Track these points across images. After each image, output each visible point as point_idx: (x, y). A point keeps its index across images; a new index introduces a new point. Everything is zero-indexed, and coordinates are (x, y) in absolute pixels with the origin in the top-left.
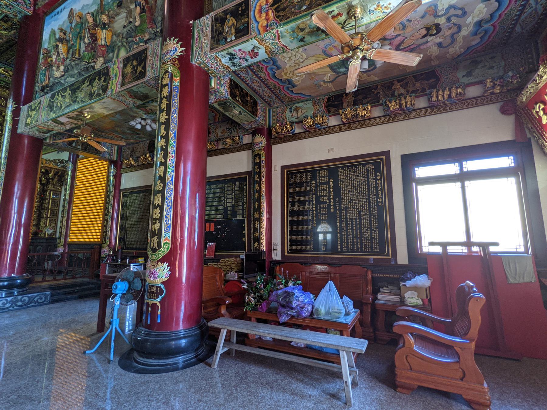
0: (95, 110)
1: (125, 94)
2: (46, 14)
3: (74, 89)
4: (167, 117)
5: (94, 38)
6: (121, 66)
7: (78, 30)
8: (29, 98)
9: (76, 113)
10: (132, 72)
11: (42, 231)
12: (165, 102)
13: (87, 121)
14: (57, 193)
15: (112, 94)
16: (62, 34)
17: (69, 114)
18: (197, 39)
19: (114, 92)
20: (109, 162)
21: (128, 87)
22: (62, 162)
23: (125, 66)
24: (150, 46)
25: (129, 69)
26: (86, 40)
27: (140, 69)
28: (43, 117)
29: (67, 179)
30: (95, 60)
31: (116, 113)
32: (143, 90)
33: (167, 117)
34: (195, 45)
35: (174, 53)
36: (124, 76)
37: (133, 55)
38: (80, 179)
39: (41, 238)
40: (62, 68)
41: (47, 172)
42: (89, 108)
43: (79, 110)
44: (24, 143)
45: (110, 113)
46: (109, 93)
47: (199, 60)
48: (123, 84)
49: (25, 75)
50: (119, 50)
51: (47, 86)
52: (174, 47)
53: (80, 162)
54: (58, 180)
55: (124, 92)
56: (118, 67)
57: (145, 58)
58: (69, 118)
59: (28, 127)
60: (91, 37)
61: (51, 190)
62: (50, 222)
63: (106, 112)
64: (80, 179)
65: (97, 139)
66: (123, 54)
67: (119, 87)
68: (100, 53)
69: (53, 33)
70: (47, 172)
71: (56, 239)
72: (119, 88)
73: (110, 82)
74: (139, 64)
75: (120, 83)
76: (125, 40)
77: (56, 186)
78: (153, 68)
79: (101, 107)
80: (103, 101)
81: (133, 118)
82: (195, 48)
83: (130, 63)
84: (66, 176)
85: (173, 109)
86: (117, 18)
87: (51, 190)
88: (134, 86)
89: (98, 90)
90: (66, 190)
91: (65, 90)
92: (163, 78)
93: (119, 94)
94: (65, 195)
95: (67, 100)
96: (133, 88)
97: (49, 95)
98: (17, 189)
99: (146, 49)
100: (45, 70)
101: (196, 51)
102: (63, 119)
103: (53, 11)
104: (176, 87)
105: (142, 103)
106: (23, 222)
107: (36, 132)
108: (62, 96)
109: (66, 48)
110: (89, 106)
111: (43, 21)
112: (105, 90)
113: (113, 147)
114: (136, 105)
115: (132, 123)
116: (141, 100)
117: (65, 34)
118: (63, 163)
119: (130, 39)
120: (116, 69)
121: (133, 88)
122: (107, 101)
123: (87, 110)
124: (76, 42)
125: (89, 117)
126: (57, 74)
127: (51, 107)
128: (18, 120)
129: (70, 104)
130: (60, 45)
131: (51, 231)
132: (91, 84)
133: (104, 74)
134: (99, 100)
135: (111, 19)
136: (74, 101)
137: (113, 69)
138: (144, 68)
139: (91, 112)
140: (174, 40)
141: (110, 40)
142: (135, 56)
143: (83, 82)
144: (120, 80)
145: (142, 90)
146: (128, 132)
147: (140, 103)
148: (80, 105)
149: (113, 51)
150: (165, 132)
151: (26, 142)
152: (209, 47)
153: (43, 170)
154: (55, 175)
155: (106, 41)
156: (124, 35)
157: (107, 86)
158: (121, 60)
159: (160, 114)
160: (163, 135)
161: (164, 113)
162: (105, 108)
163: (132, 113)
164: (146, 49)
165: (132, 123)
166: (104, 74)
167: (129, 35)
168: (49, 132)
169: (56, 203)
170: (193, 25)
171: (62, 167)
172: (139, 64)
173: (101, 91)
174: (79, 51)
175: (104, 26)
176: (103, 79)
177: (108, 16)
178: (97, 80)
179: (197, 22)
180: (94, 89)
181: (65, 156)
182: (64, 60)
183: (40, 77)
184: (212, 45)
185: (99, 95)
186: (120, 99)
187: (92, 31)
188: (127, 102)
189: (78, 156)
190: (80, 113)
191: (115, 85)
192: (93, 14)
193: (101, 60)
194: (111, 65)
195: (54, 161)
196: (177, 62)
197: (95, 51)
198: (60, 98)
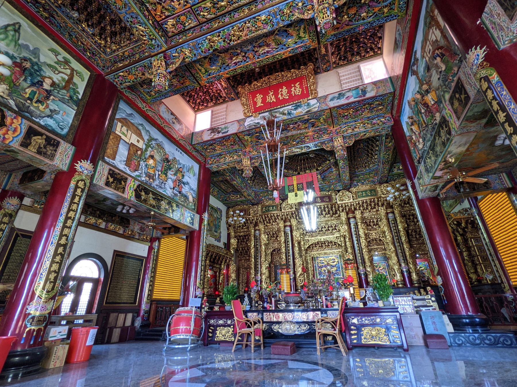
0: (454, 152)
1: (466, 124)
2: (399, 116)
3: (432, 148)
4: (505, 114)
5: (426, 105)
6: (450, 107)
7: (416, 109)
8: (415, 173)
9: (443, 164)
10: (459, 104)
11: (482, 277)
12: (494, 103)
13: (455, 165)
14: (478, 239)
15: (456, 132)
16: (411, 120)
17: (439, 167)
18: (492, 28)
19: (456, 129)
20: (506, 192)
21: (463, 117)
22: (466, 210)
23: (452, 104)
24: (461, 74)
25: (456, 104)
26: (423, 111)
27: (463, 97)
28: (427, 180)
29: (478, 224)
30: (434, 118)
31: (471, 145)
32: (478, 109)
33: (505, 114)
34: (494, 33)
35: (478, 60)
36: (456, 112)
37: (453, 92)
38: (489, 219)
39: (485, 285)
40: (421, 140)
41: (459, 224)
42: (449, 153)
43: (443, 160)
44: (427, 204)
45: (466, 147)
46: (453, 133)
47: (506, 41)
48: (458, 118)
49: (407, 160)
50: (444, 97)
51: (420, 158)
52: (477, 54)
53: (481, 204)
54: (472, 228)
55: (464, 123)
56: (449, 110)
57: (462, 85)
58: (441, 170)
59: (423, 192)
60: (424, 106)
61: (471, 238)
62: (485, 268)
63: (463, 149)
64: (489, 219)
65: (471, 174)
66: (447, 96)
67: (457, 122)
68: (434, 110)
69: (407, 123)
70: (459, 224)
71: (498, 284)
72: (458, 123)
73: (450, 124)
74: (460, 94)
75: (456, 120)
76: (444, 87)
77: (473, 234)
78: (471, 86)
79: (456, 147)
80: (453, 142)
81: (495, 138)
82: (495, 36)
83: (455, 99)
84: (476, 222)
85: (506, 103)
86: (432, 79)
87: (471, 238)
88: (467, 112)
89: (446, 135)
90: (482, 233)
91: (428, 152)
92: (481, 86)
93: (461, 127)
94: (484, 239)
95: (433, 158)
96: (467, 115)
97: (423, 163)
98: (438, 239)
99: (459, 79)
100: (414, 149)
101: (498, 37)
102: (439, 174)
103: (401, 111)
104: (497, 82)
105: (487, 119)
106: (457, 270)
107: (430, 193)
108: (429, 158)
109: (417, 126)
110: (447, 153)
111: (400, 120)
112: (449, 133)
113: (500, 176)
114: (483, 125)
115: (499, 142)
116: (484, 118)
117: (412, 118)
118: (468, 211)
119: (447, 83)
120: (448, 112)
121: (467, 115)
122: (456, 139)
123: (449, 156)
124: (419, 117)
125: (453, 161)
126: (420, 146)
127: (427, 171)
128: (416, 191)
129: (436, 160)
130: (413, 127)
131: (491, 277)
132: (440, 136)
133: (443, 123)
134: (450, 143)
135: (429, 83)
136: (437, 156)
137: (447, 113)
138: (466, 93)
139: (452, 156)
140: (471, 51)
141: (435, 97)
142: (454, 92)
143: (435, 138)
144: (455, 117)
145: (476, 110)
146: (504, 153)
147: (484, 121)
148: (442, 156)
149: (441, 102)
150: (512, 128)
151: (428, 203)
152: (507, 20)
153: (455, 223)
154: (467, 223)
155: (433, 100)
156: (442, 84)
157: (450, 129)
158: (447, 102)
159: (497, 116)
160: (512, 132)
161: (500, 112)
162: (460, 146)
163: (492, 135)
164: (459, 79)
165: (499, 142)
166: (444, 122)
167: (445, 81)
168: (437, 189)
169: (481, 249)
170: (483, 22)
171: (468, 214)
172: (460, 94)
173: (448, 136)
174: (424, 121)
175: (427, 92)
176: (444, 127)
177: (426, 83)
178: (442, 131)
179: (484, 15)
180: (443, 138)
181: (466, 204)
182: (419, 134)
183: (414, 155)
184: (509, 16)
185: (448, 139)
186: (465, 130)
187: (423, 102)
188: (473, 129)
189: (476, 198)
190: (446, 162)
191: (454, 123)
192: (418, 92)
193: (438, 115)
194: (444, 112)
195: (459, 212)
196: (485, 64)
197: (432, 113)
198: (429, 160)
